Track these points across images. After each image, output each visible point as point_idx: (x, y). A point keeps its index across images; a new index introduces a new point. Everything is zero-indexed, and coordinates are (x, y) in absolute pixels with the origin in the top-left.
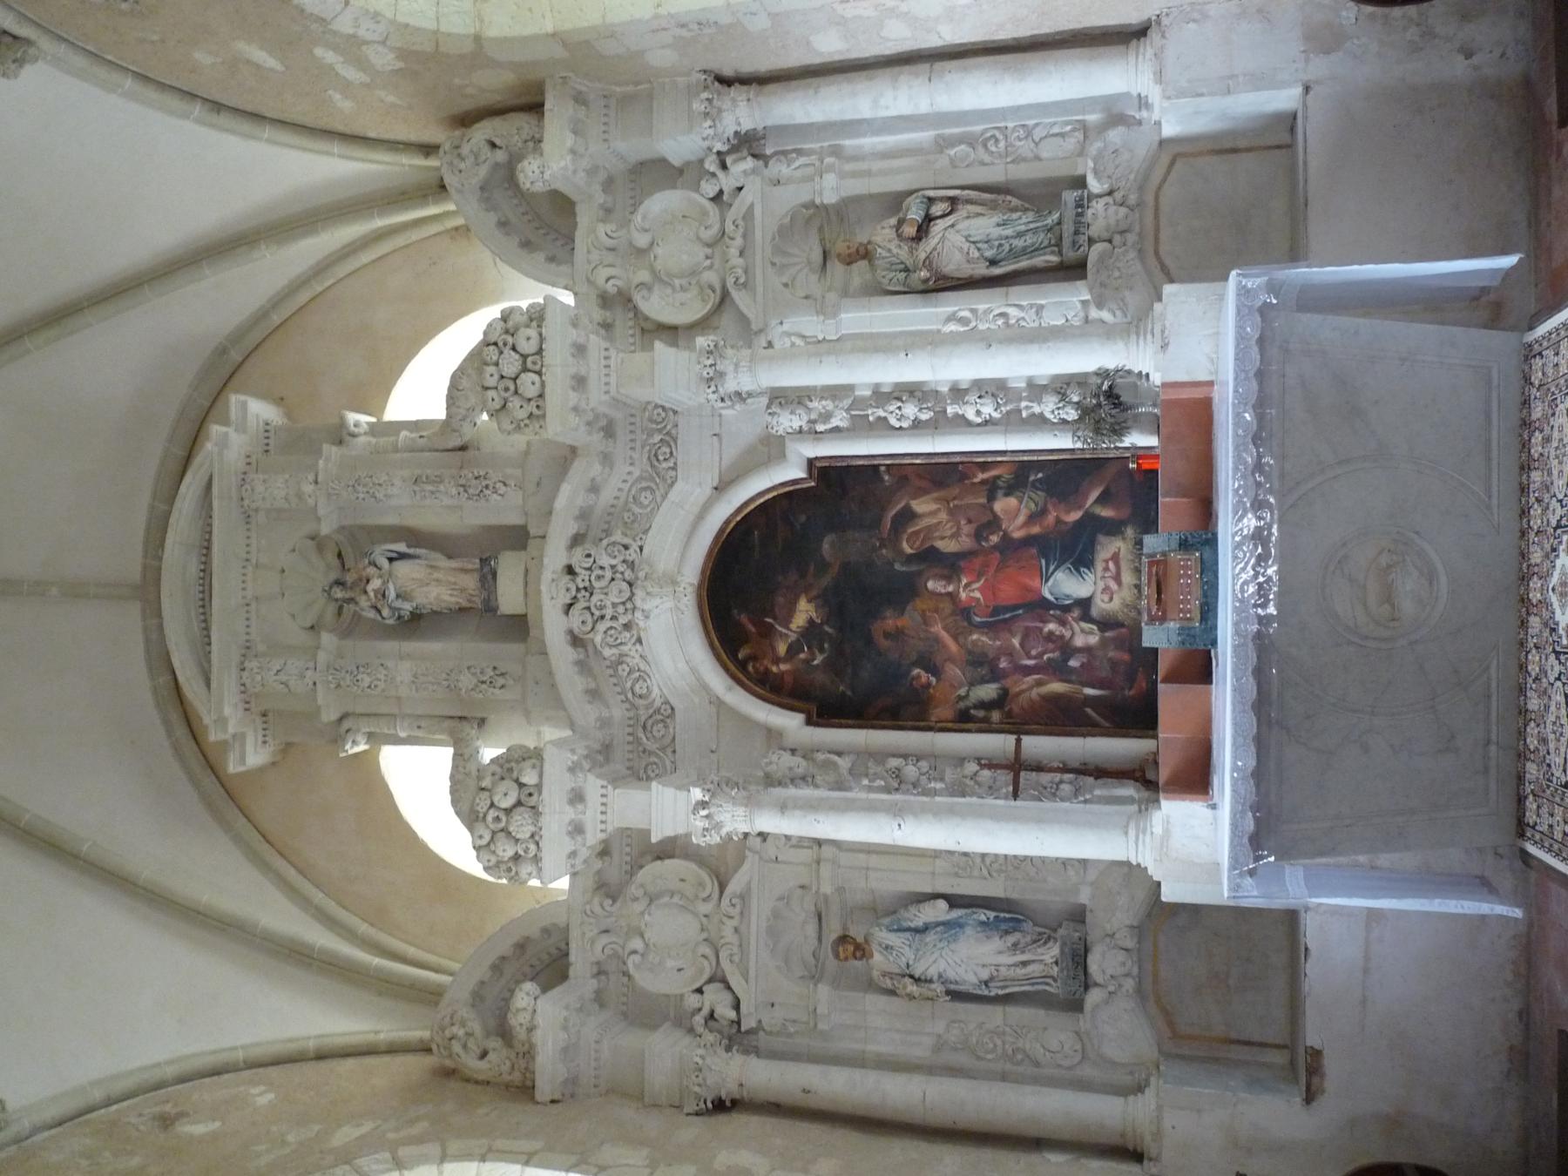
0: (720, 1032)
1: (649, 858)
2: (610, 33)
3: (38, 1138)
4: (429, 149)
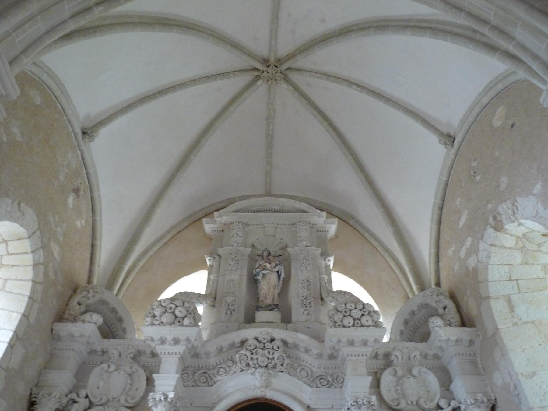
1: (148, 374)
2: (504, 354)
3: (79, 152)
4: (438, 284)
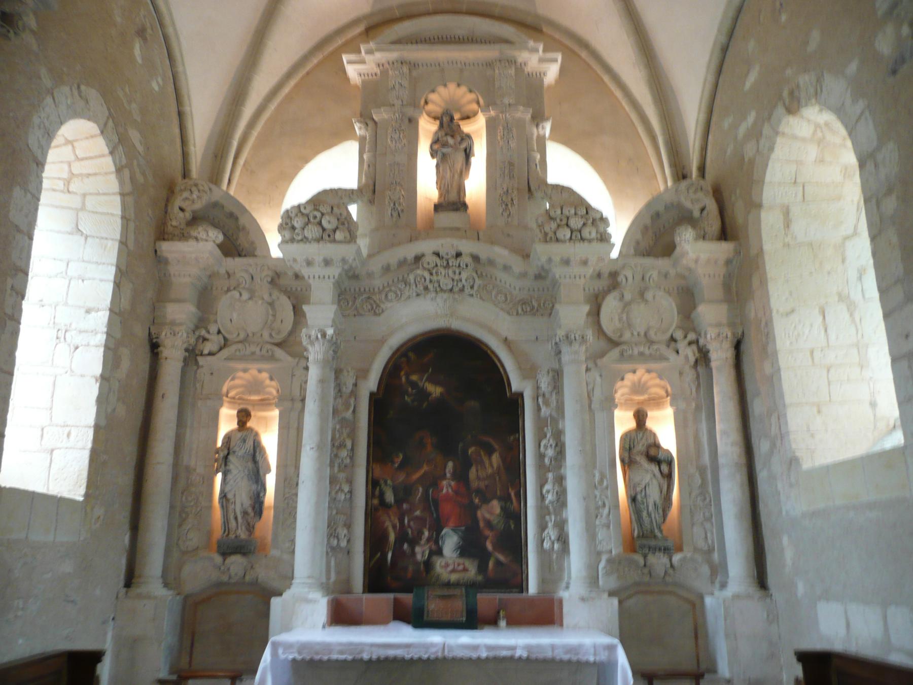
0: (196, 345)
2: (764, 282)
4: (702, 170)
